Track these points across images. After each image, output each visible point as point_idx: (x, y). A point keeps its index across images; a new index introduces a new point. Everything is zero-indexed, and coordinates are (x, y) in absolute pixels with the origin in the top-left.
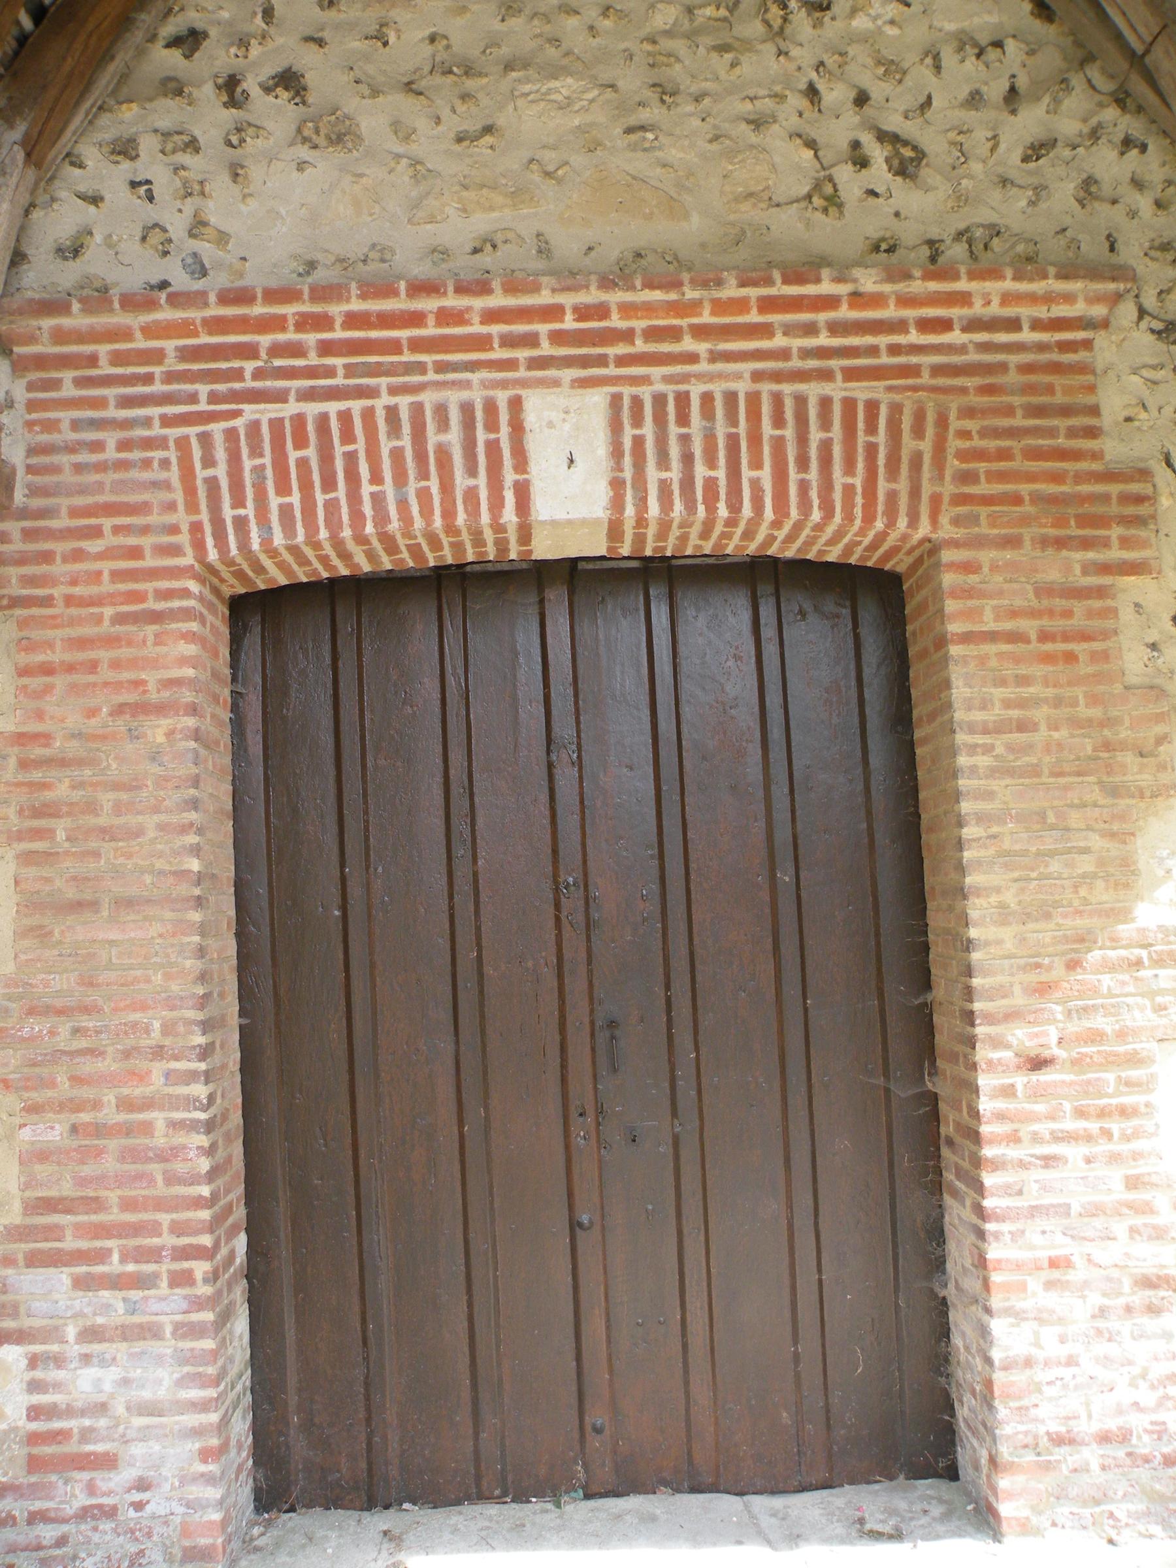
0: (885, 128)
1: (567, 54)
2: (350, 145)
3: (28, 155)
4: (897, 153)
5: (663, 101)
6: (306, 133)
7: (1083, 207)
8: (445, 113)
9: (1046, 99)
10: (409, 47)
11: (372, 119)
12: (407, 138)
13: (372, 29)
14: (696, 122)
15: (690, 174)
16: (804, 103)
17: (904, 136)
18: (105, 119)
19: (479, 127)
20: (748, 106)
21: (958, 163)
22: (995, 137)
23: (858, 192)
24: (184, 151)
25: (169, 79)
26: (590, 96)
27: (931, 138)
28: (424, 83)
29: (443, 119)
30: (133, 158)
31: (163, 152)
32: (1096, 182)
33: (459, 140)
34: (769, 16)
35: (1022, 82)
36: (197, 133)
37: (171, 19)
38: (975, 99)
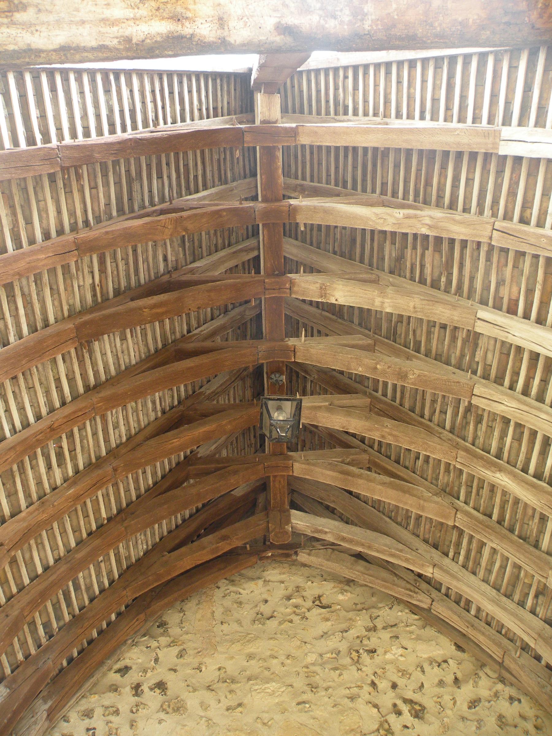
0: (406, 697)
1: (273, 674)
2: (182, 712)
3: (48, 715)
4: (413, 708)
5: (312, 691)
6: (164, 707)
7: (502, 729)
8: (223, 698)
9: (471, 682)
10: (210, 672)
11: (192, 701)
12: (206, 709)
13: (196, 666)
14: (326, 699)
15: (325, 722)
16: (371, 689)
17: (415, 700)
18: (84, 701)
19: (236, 704)
20: (348, 691)
21: (440, 711)
22: (454, 699)
23: (399, 727)
24: (112, 715)
25: (113, 685)
26: (282, 690)
27: (427, 700)
28: (215, 686)
29: (222, 701)
30: (90, 718)
31: (104, 715)
32: (504, 717)
33: (228, 710)
34: (352, 656)
35: (459, 675)
36: (120, 707)
37: (119, 663)
38: (441, 683)
